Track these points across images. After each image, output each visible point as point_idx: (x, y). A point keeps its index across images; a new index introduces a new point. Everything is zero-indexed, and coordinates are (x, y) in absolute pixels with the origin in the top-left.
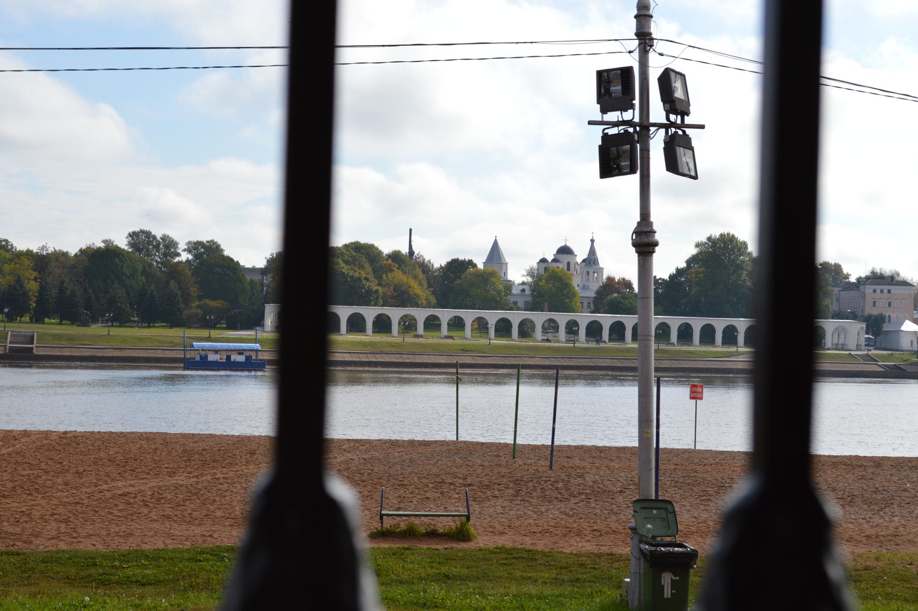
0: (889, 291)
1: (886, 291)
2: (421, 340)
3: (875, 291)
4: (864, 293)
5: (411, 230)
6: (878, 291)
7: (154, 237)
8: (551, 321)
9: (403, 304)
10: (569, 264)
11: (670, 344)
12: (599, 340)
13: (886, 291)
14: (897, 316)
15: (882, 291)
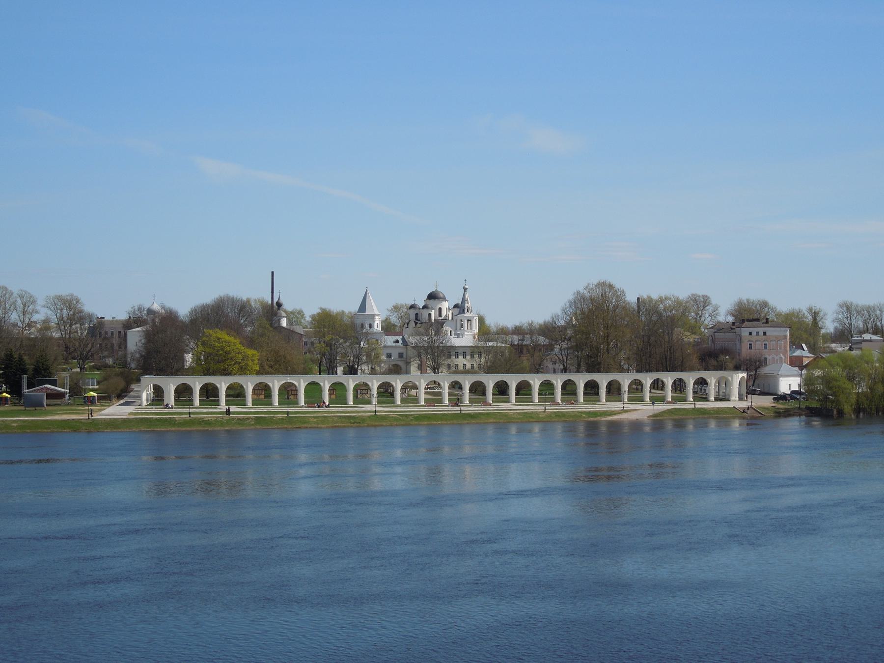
0: (765, 333)
1: (761, 334)
3: (750, 334)
4: (740, 336)
7: (12, 293)
8: (681, 380)
9: (674, 369)
10: (440, 309)
11: (487, 404)
12: (190, 402)
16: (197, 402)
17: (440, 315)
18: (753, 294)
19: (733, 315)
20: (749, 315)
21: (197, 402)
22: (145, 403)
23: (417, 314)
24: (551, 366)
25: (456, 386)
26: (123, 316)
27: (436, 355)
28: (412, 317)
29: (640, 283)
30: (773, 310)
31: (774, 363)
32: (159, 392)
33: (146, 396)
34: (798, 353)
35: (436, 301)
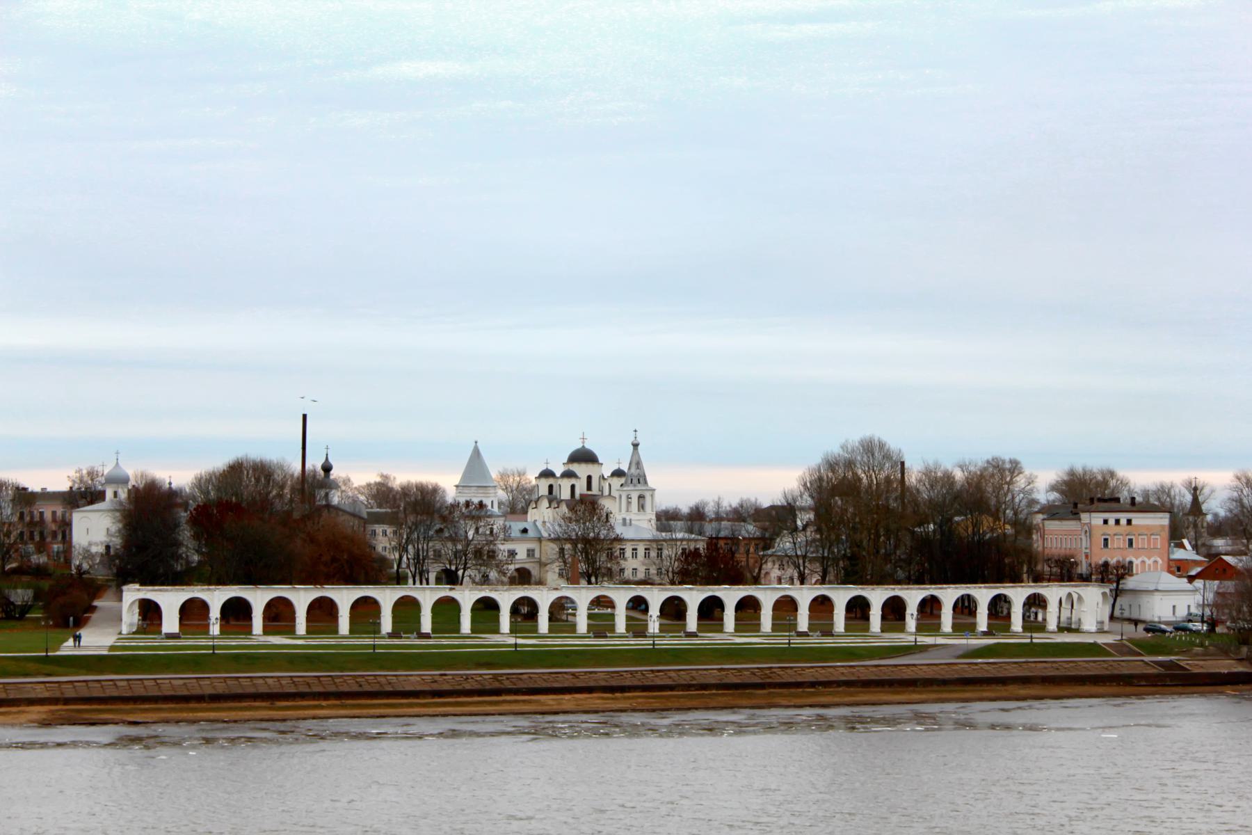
0: (1129, 522)
1: (1123, 522)
2: (431, 642)
3: (1106, 522)
5: (305, 417)
6: (1112, 522)
10: (589, 478)
13: (1123, 522)
14: (1143, 562)
15: (1117, 522)
16: (215, 629)
17: (589, 487)
18: (1091, 461)
19: (1062, 492)
20: (1086, 494)
21: (215, 629)
22: (125, 630)
23: (551, 487)
24: (775, 573)
25: (638, 604)
26: (60, 483)
27: (590, 552)
28: (544, 491)
29: (935, 444)
30: (1124, 483)
31: (1143, 571)
32: (150, 611)
33: (130, 618)
34: (1179, 554)
35: (596, 466)
